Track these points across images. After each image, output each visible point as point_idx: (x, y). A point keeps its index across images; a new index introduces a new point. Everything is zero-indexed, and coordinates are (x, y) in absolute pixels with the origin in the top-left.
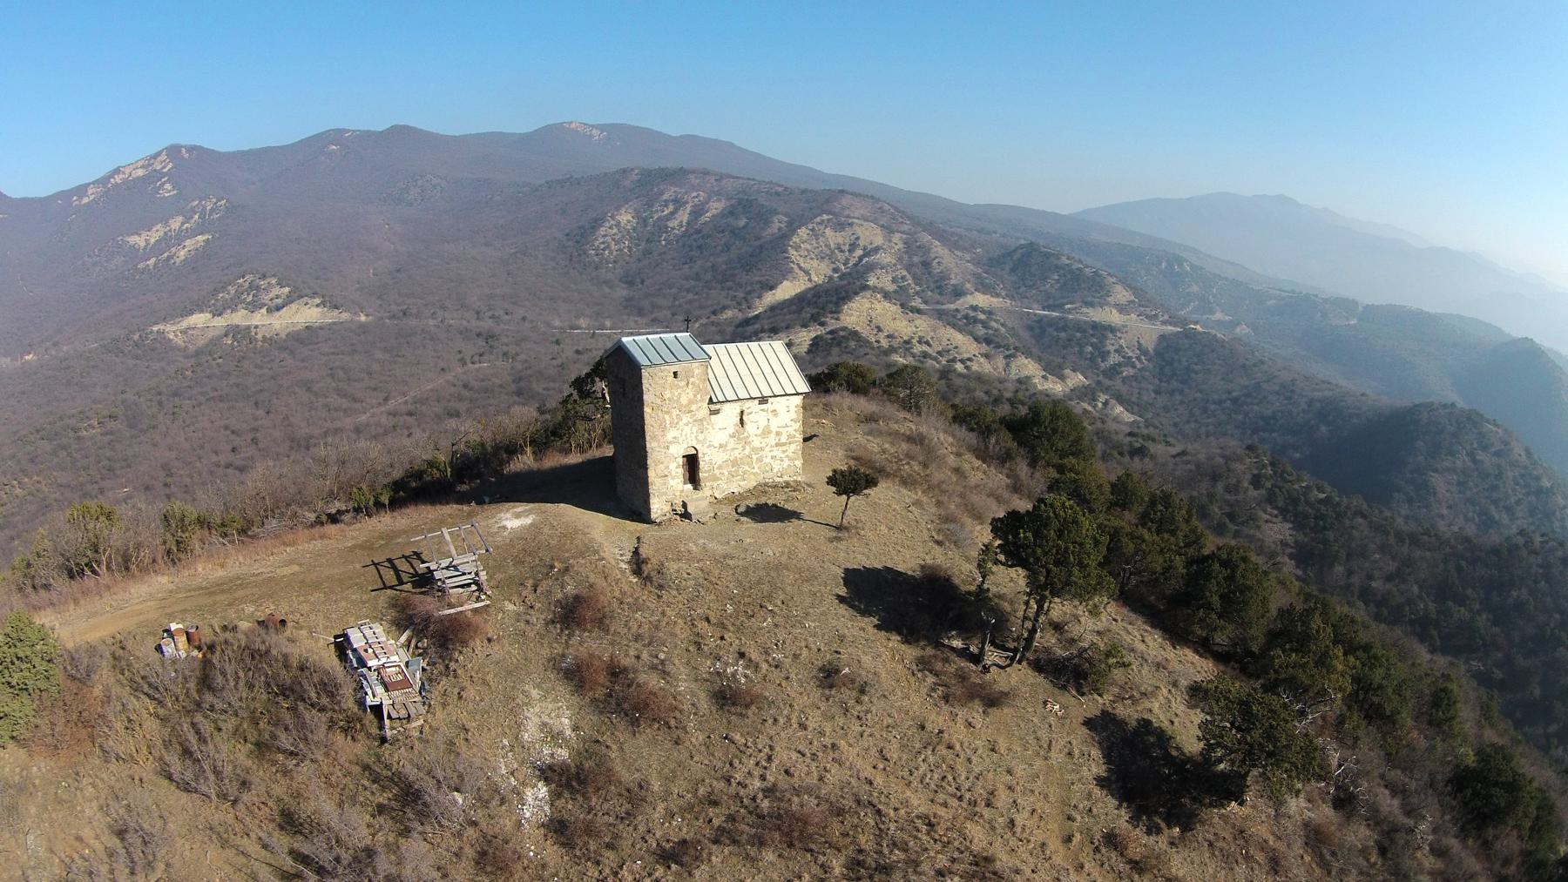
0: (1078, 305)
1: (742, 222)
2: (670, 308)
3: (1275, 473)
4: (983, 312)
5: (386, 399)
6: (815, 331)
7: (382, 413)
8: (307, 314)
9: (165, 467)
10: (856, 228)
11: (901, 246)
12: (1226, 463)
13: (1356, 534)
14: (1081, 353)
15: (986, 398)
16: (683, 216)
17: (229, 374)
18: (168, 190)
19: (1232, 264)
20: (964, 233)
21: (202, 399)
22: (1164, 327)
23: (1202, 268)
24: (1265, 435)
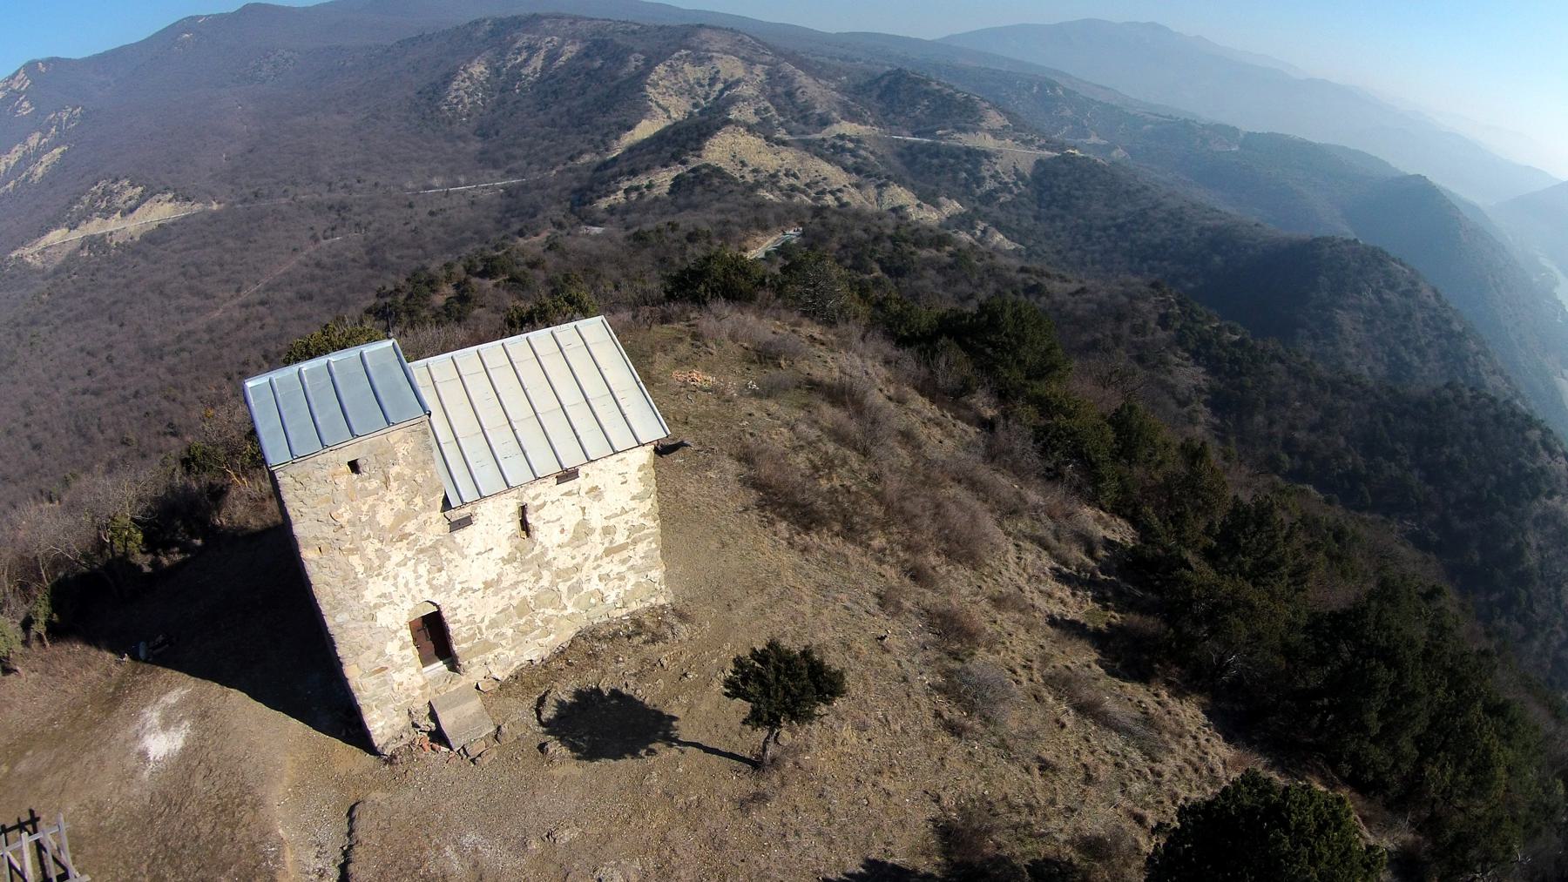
0: (950, 130)
1: (598, 63)
2: (525, 158)
3: (1184, 313)
4: (851, 140)
5: (239, 290)
6: (677, 170)
7: (234, 306)
8: (161, 211)
9: (25, 405)
10: (715, 61)
11: (763, 77)
12: (1130, 302)
13: (1275, 380)
14: (955, 179)
15: (865, 236)
16: (537, 62)
17: (83, 289)
18: (26, 108)
19: (1102, 87)
20: (827, 60)
21: (58, 322)
22: (1040, 152)
23: (1074, 92)
24: (1156, 263)
